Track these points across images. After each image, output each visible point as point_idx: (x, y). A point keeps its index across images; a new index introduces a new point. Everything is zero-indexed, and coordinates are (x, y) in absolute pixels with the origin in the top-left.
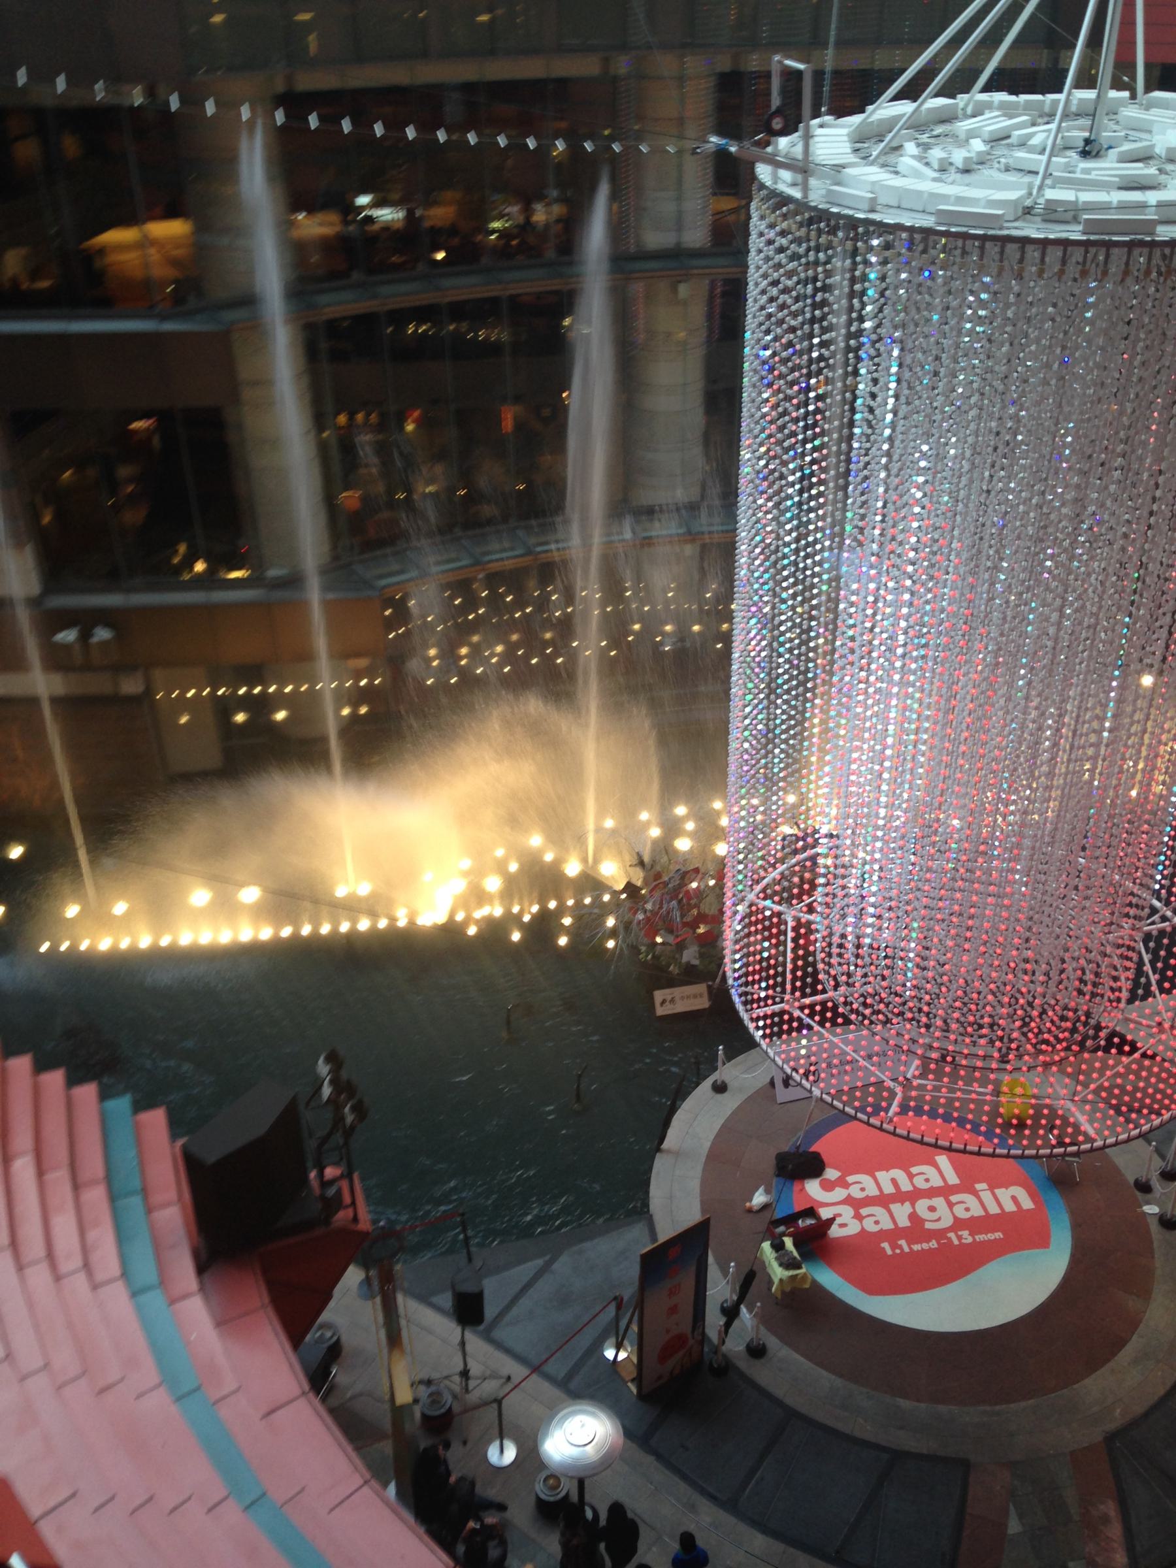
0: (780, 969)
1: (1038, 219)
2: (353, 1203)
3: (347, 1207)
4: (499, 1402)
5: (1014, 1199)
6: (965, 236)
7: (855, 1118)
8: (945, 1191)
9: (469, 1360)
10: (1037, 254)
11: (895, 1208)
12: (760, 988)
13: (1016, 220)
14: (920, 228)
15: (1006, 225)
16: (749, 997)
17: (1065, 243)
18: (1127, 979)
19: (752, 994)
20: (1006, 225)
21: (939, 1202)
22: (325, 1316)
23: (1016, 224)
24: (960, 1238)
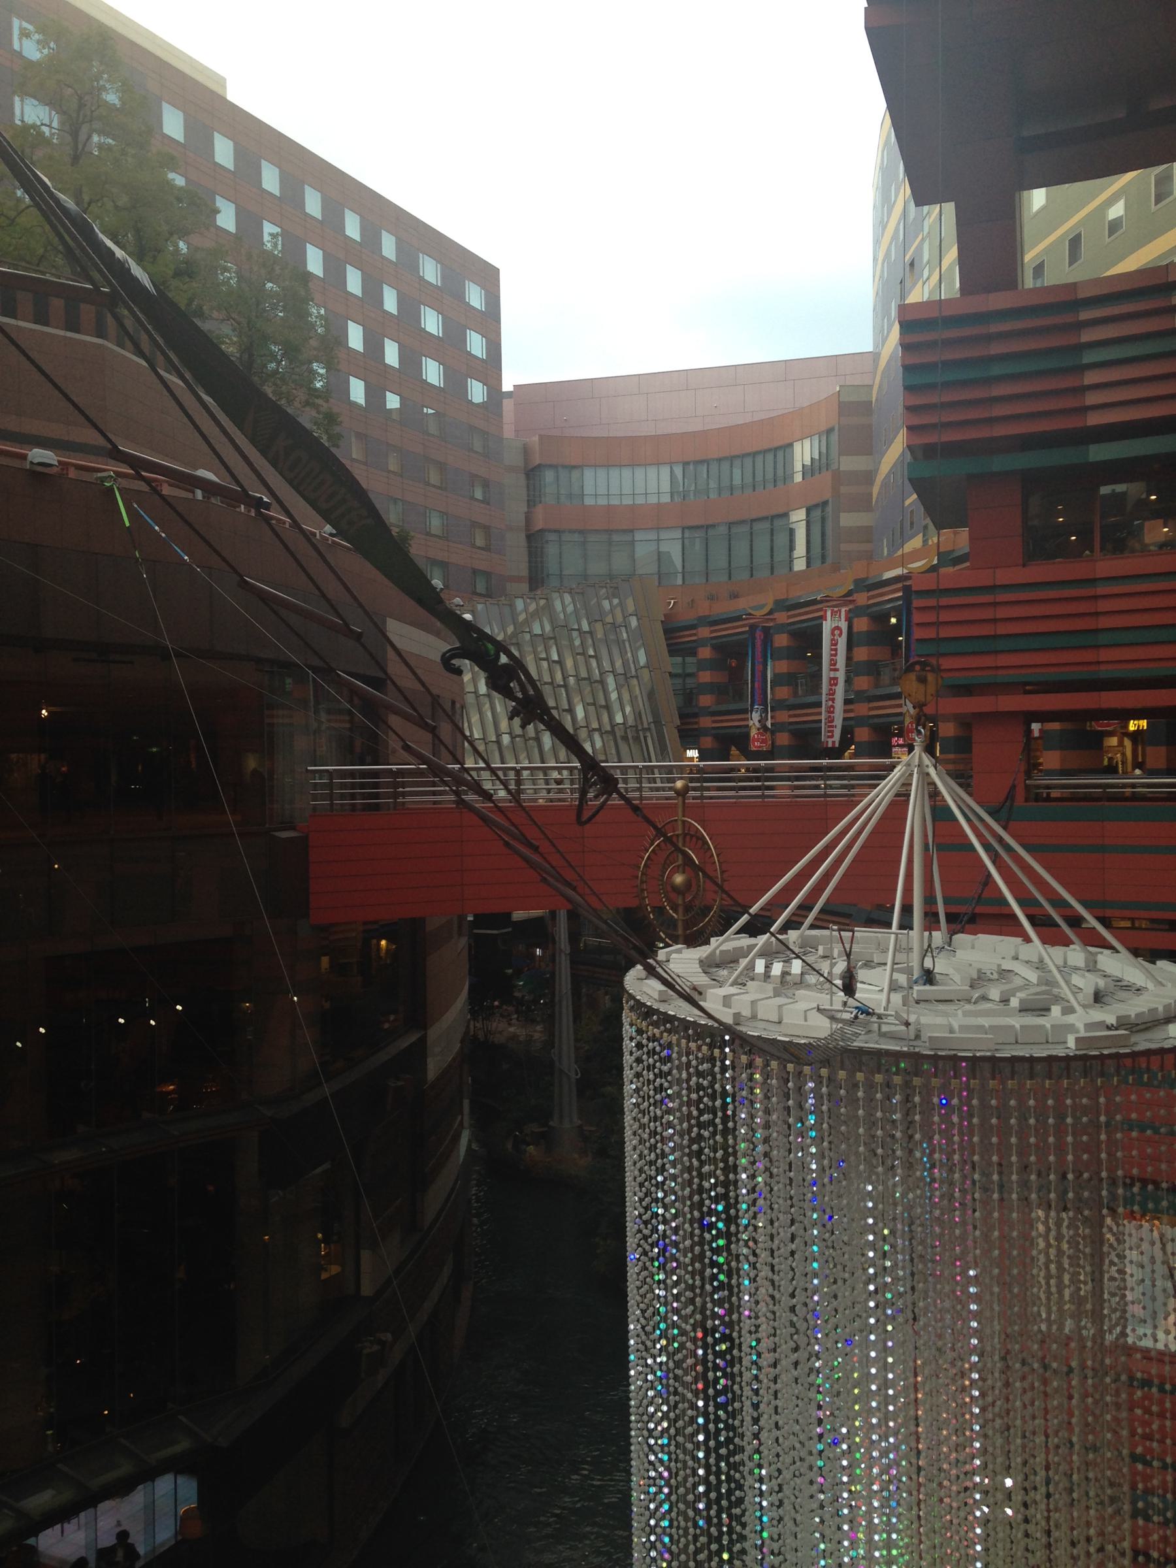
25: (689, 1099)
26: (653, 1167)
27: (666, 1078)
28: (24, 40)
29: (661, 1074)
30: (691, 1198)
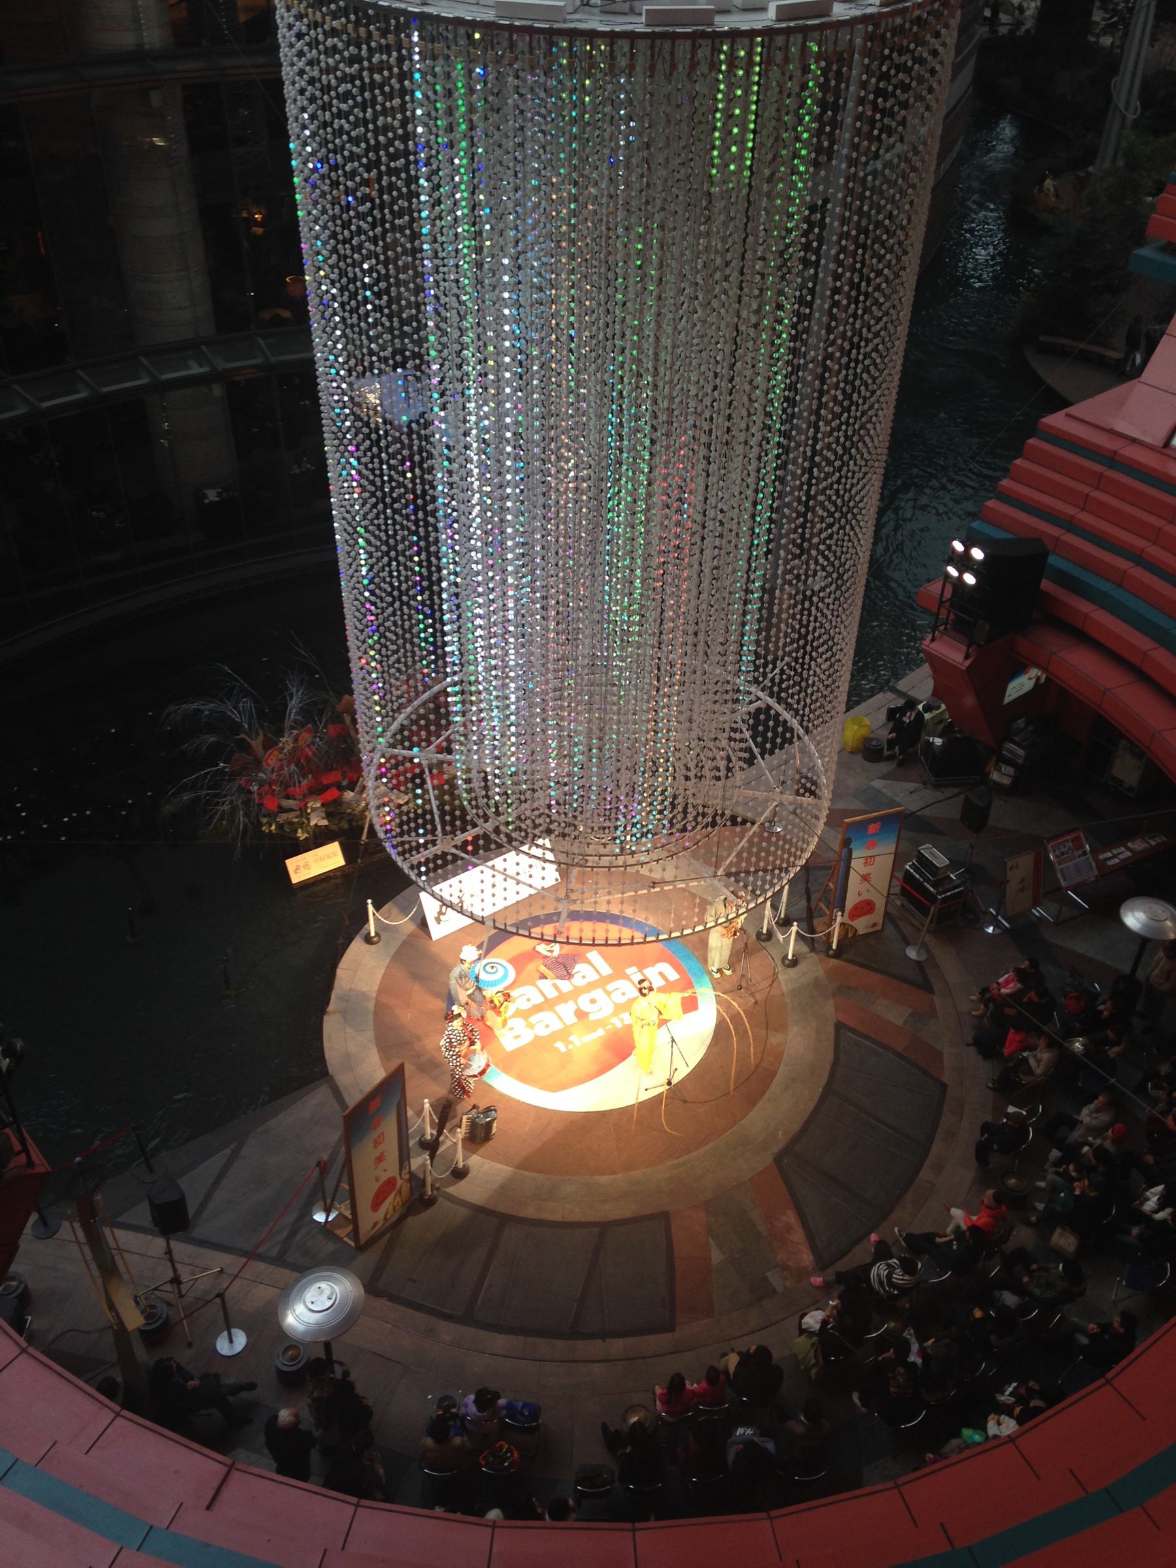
0: (428, 817)
1: (596, 10)
2: (25, 1150)
3: (19, 1153)
4: (221, 1296)
5: (661, 974)
6: (530, 30)
7: (517, 934)
8: (603, 982)
9: (178, 1266)
10: (626, 49)
11: (560, 1008)
12: (418, 835)
13: (575, 12)
14: (482, 22)
15: (568, 17)
16: (407, 846)
17: (632, 36)
18: (722, 758)
19: (409, 842)
20: (568, 17)
21: (598, 993)
22: (14, 1268)
23: (577, 16)
24: (622, 1020)
25: (372, 81)
26: (329, 129)
27: (359, 161)
28: (862, 861)
29: (340, 115)
30: (385, 231)
